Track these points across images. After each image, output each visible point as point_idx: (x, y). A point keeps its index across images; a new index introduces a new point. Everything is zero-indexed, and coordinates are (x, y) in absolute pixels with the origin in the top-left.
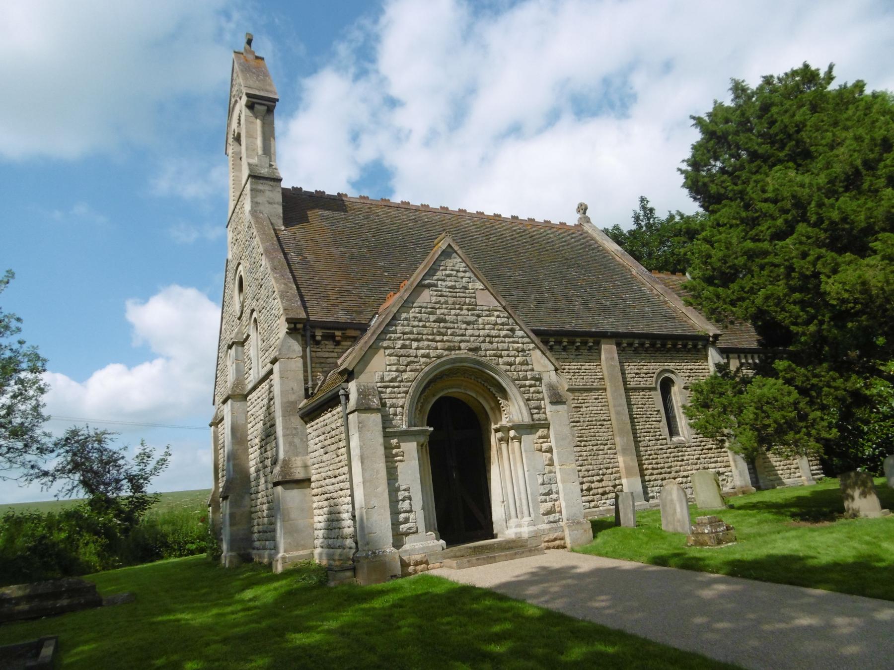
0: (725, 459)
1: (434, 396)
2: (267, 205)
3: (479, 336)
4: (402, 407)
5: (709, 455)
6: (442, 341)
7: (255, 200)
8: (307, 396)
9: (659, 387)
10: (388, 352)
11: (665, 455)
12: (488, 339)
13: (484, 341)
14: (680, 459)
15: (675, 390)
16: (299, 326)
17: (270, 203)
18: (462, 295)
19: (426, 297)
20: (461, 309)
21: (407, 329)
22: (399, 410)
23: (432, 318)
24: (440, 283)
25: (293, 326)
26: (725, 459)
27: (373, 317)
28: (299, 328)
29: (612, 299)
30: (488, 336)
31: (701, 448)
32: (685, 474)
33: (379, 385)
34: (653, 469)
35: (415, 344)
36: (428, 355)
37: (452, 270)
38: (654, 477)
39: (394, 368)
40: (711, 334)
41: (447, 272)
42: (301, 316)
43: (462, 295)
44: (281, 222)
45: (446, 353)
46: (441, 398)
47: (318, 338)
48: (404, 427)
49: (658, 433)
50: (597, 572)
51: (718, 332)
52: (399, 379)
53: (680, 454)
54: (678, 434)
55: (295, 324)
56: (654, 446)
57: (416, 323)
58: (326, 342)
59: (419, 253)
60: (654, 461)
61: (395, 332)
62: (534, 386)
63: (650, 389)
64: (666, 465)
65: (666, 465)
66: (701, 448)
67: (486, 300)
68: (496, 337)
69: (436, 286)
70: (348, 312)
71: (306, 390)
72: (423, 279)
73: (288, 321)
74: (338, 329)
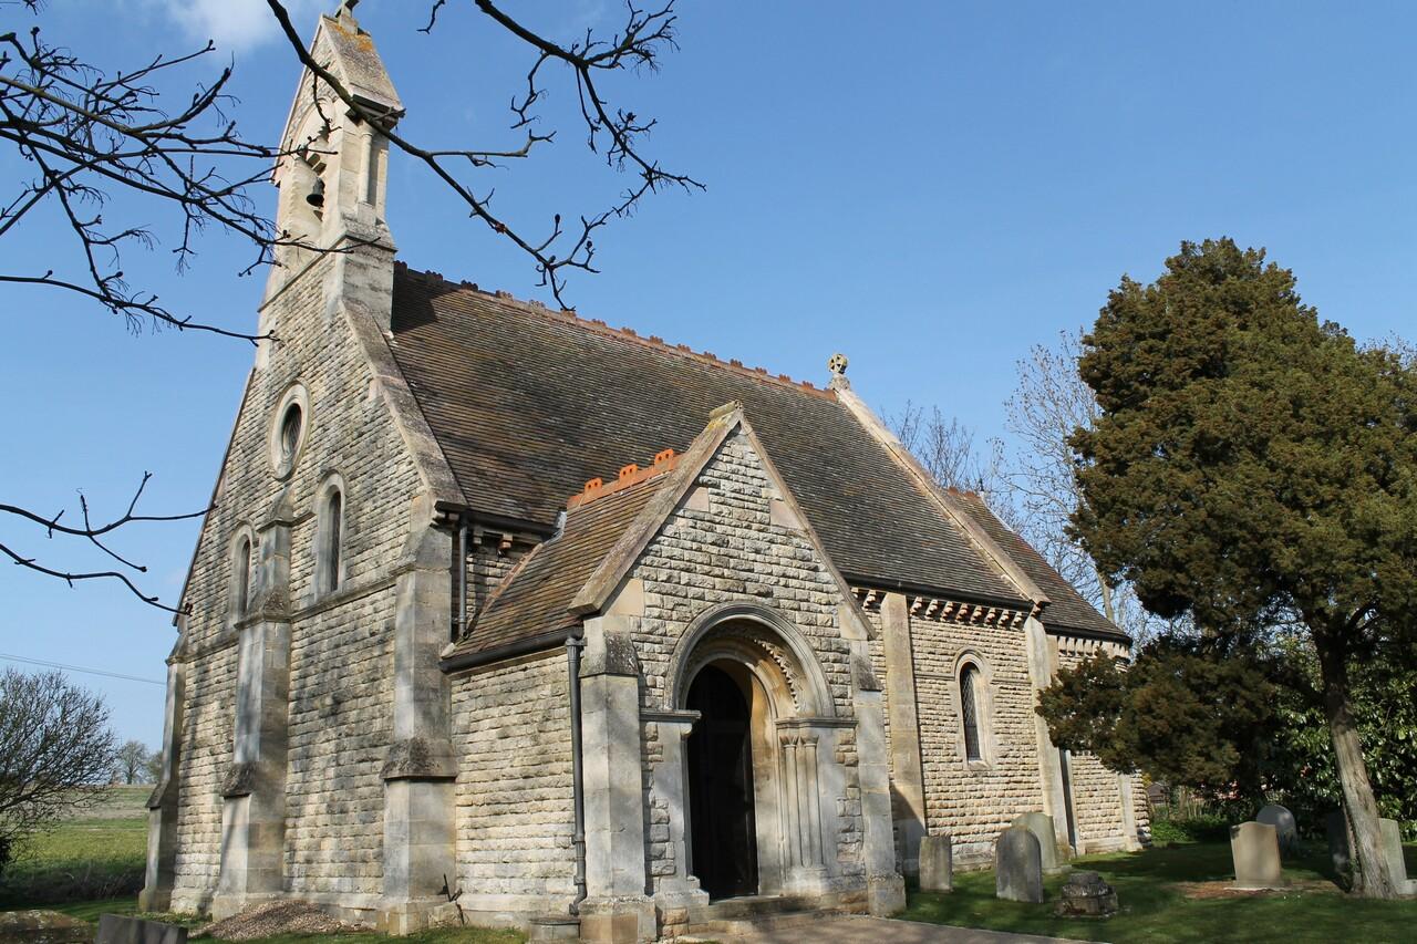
0: (1037, 799)
1: (698, 662)
2: (369, 291)
3: (771, 574)
4: (664, 675)
5: (1017, 792)
6: (722, 576)
7: (351, 280)
8: (454, 636)
9: (958, 677)
10: (648, 584)
11: (958, 788)
12: (783, 581)
13: (777, 583)
14: (978, 794)
15: (977, 681)
16: (453, 517)
17: (373, 289)
18: (751, 505)
19: (701, 501)
20: (749, 527)
21: (677, 552)
22: (660, 679)
23: (710, 537)
24: (723, 482)
25: (442, 515)
26: (1037, 799)
27: (559, 515)
28: (451, 518)
29: (895, 525)
30: (784, 576)
31: (1007, 779)
32: (983, 818)
33: (634, 636)
34: (942, 807)
35: (685, 577)
36: (711, 597)
37: (740, 464)
38: (941, 821)
39: (656, 612)
40: (1037, 602)
41: (734, 467)
42: (460, 502)
43: (751, 505)
44: (386, 323)
45: (727, 595)
46: (707, 666)
47: (478, 541)
48: (667, 708)
49: (951, 752)
50: (1182, 880)
51: (1046, 599)
52: (661, 631)
53: (979, 786)
54: (977, 756)
55: (447, 512)
56: (946, 771)
57: (688, 544)
58: (486, 549)
59: (604, 408)
60: (943, 796)
61: (658, 554)
62: (840, 661)
63: (947, 679)
64: (959, 803)
65: (959, 803)
66: (1007, 779)
67: (789, 516)
68: (793, 578)
69: (716, 486)
70: (521, 503)
71: (455, 627)
72: (701, 474)
73: (440, 507)
74: (508, 529)
